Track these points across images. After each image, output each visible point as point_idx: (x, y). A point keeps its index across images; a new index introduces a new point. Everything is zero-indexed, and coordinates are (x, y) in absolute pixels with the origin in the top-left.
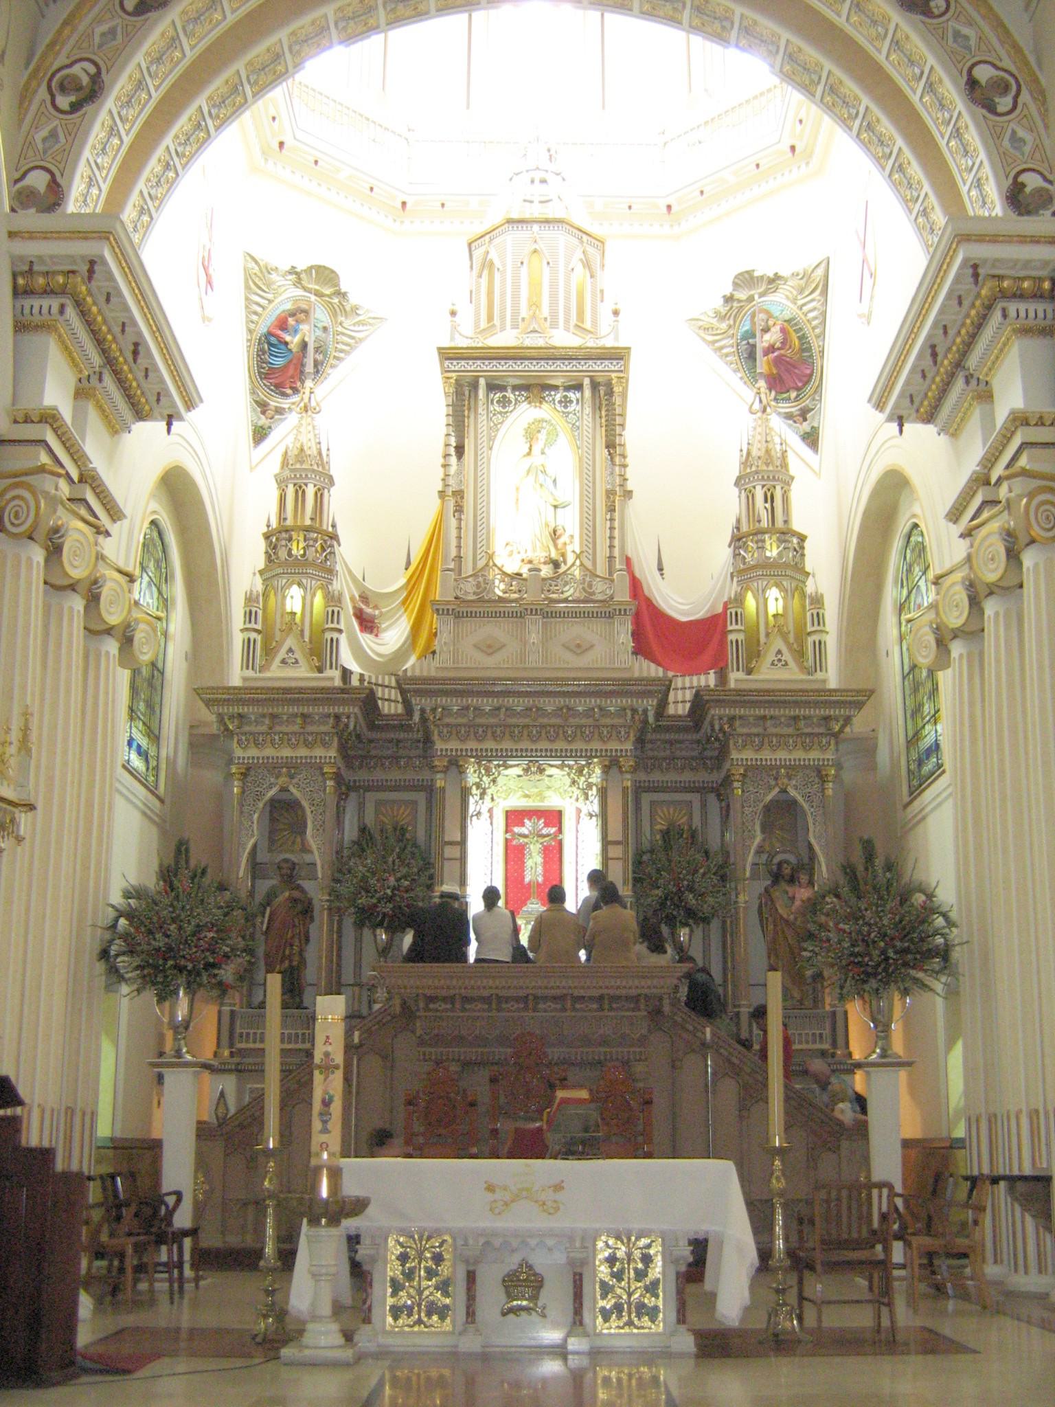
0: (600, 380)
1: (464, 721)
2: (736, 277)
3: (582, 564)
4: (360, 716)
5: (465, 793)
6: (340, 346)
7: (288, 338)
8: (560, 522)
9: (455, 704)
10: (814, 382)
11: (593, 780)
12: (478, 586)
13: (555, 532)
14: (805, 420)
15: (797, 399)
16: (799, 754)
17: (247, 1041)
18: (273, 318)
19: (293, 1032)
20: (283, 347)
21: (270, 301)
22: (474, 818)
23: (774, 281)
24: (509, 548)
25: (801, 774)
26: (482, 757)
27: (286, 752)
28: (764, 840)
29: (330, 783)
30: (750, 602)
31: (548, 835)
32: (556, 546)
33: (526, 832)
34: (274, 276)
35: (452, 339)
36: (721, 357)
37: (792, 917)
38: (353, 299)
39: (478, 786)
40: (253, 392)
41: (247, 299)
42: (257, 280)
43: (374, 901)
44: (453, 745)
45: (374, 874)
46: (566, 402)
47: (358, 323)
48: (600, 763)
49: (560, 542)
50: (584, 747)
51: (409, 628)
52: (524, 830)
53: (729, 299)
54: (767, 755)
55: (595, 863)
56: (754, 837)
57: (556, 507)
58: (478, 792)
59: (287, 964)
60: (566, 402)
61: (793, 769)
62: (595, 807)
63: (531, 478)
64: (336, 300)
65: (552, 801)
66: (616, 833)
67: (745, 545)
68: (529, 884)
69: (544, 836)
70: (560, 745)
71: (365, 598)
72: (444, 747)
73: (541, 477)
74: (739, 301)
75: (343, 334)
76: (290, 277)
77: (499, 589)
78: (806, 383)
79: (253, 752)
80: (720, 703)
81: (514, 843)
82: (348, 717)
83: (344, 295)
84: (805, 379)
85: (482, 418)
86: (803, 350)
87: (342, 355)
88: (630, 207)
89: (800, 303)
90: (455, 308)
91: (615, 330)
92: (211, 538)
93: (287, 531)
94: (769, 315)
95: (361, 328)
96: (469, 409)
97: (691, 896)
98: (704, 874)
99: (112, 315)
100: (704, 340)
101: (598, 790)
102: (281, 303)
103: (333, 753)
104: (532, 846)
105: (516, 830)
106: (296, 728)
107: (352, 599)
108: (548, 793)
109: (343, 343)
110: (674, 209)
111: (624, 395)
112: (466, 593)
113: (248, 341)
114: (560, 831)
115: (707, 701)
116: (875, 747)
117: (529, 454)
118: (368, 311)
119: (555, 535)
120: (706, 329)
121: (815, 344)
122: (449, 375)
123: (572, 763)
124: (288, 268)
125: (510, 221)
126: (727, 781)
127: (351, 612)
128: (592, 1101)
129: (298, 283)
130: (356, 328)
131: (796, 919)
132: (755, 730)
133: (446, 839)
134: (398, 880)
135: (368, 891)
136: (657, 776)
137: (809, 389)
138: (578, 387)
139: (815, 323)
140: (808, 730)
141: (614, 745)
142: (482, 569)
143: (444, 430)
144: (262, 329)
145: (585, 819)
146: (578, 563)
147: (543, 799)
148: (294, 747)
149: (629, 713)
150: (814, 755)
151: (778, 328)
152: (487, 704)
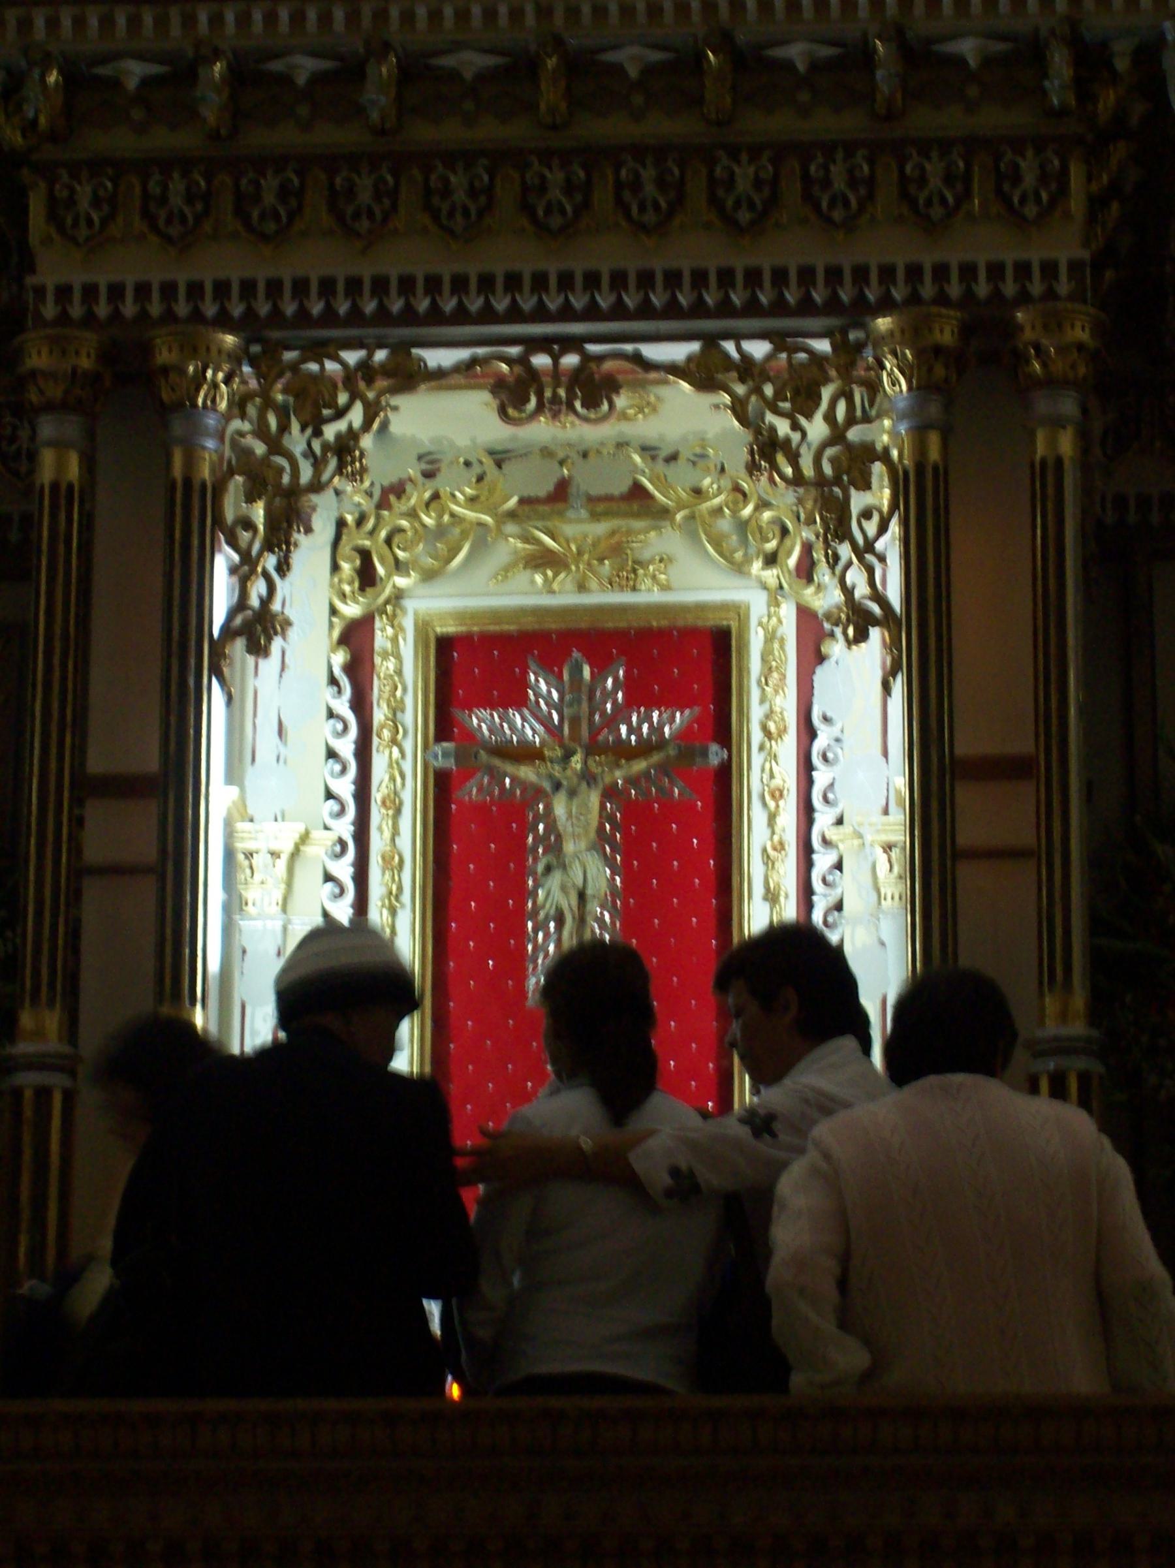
1: (185, 140)
31: (645, 748)
33: (533, 733)
48: (913, 333)
55: (778, 697)
58: (258, 513)
69: (623, 752)
72: (78, 279)
81: (472, 791)
96: (906, 473)
99: (187, 210)
104: (560, 809)
105: (481, 721)
123: (758, 349)
133: (97, 764)
149: (1060, 62)
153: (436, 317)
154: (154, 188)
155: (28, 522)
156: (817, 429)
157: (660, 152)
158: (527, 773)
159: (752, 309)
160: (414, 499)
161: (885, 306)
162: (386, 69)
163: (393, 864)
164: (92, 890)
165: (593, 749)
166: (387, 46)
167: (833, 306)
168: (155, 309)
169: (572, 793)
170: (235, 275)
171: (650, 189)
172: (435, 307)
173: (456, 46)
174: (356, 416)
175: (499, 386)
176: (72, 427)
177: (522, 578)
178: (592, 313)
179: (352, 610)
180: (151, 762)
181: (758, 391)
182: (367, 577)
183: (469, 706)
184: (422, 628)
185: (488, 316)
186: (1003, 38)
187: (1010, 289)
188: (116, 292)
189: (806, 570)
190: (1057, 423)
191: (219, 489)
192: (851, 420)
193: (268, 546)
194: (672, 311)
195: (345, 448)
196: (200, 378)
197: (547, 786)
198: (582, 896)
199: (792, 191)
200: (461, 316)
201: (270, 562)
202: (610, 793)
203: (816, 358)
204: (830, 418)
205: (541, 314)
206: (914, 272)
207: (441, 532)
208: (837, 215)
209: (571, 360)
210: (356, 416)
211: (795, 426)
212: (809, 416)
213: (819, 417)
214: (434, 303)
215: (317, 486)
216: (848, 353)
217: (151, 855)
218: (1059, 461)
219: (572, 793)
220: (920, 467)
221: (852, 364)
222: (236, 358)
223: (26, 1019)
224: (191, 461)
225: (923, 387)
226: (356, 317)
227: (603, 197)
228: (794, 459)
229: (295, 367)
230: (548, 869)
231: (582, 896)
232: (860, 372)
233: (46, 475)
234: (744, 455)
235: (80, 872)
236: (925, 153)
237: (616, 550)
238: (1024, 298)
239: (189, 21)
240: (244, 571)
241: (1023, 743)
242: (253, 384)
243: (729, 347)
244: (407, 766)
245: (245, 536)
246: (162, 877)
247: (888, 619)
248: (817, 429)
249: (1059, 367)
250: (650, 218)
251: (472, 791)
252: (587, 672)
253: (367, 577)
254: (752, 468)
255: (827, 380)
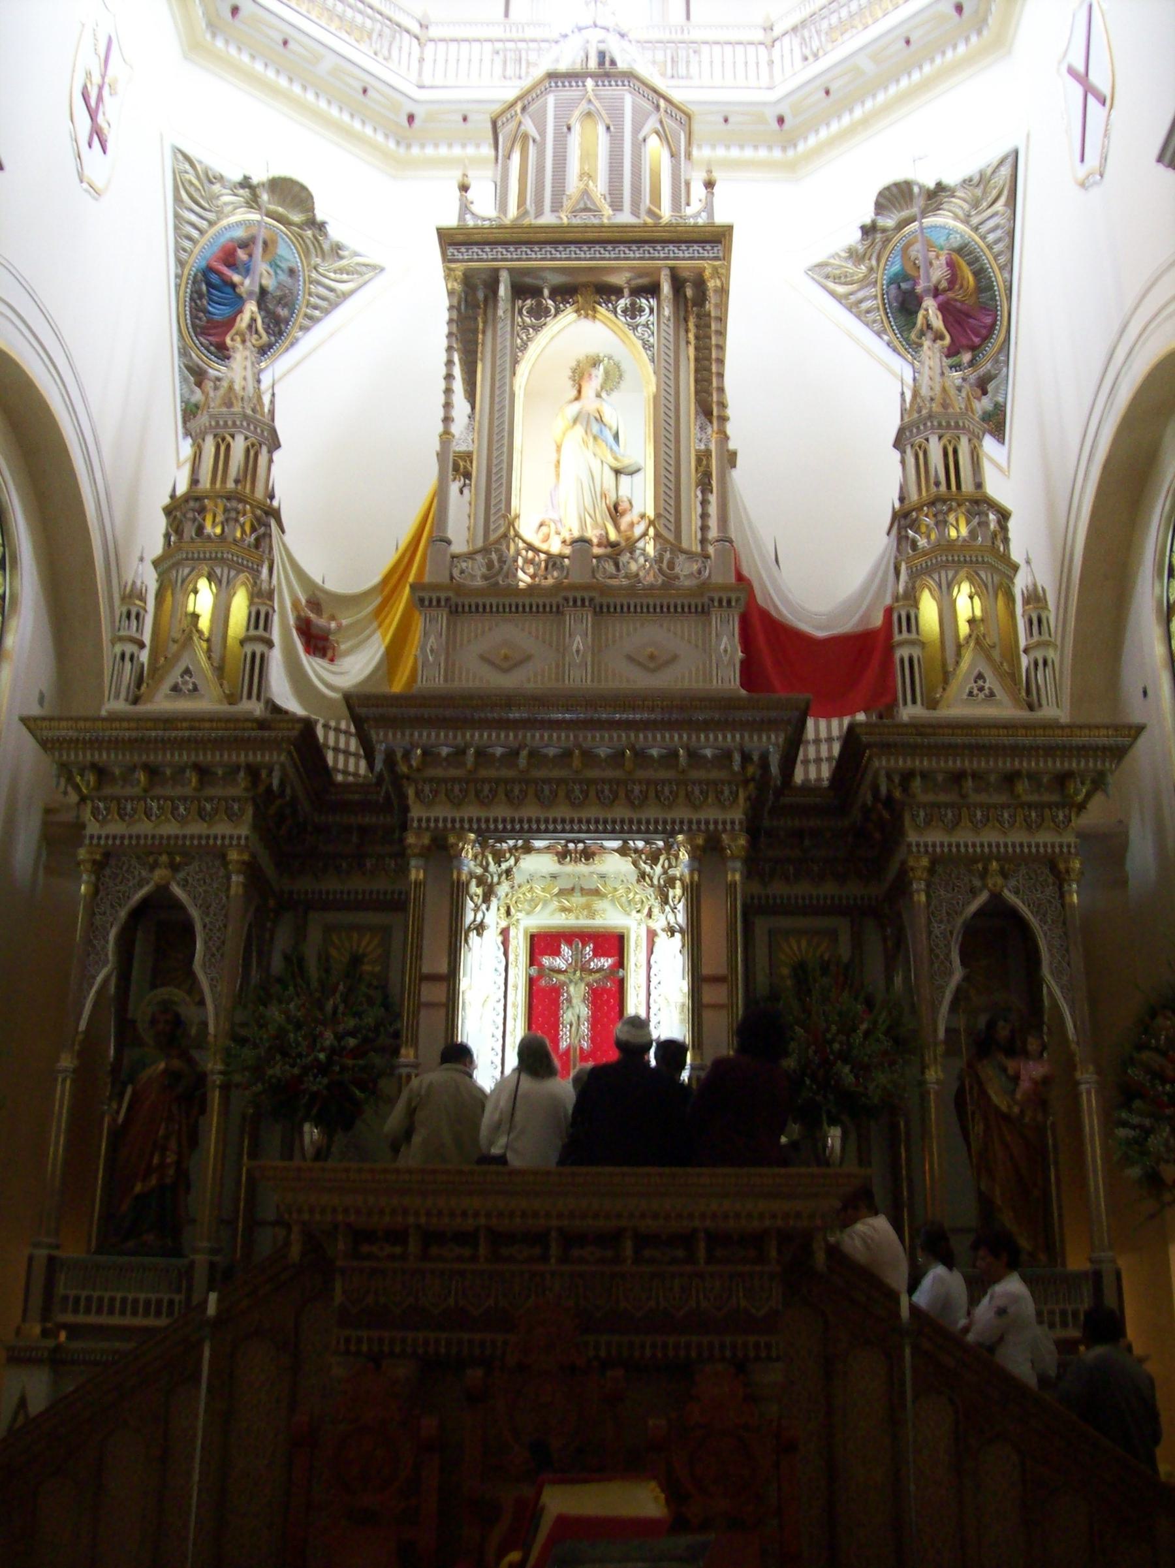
0: (686, 274)
2: (881, 194)
3: (658, 535)
4: (291, 771)
5: (457, 893)
6: (313, 300)
7: (236, 278)
8: (624, 492)
9: (444, 742)
10: (999, 337)
11: (676, 872)
12: (490, 565)
13: (616, 507)
14: (985, 393)
15: (972, 363)
16: (1018, 836)
17: (76, 1311)
18: (215, 249)
19: (153, 1297)
20: (229, 290)
21: (211, 224)
22: (473, 935)
23: (937, 195)
24: (544, 529)
25: (1023, 870)
26: (487, 834)
27: (170, 828)
28: (966, 978)
29: (236, 879)
30: (929, 610)
32: (617, 526)
33: (563, 966)
34: (217, 188)
35: (461, 217)
36: (858, 317)
37: (1016, 1110)
38: (335, 232)
39: (481, 881)
40: (184, 353)
41: (177, 216)
42: (192, 190)
43: (296, 1071)
44: (441, 811)
45: (298, 1026)
46: (633, 311)
47: (341, 271)
48: (690, 840)
49: (624, 522)
50: (661, 815)
51: (382, 649)
52: (559, 963)
53: (868, 231)
54: (964, 837)
56: (951, 973)
57: (617, 472)
58: (479, 891)
59: (153, 1181)
60: (633, 311)
61: (1010, 862)
62: (681, 918)
63: (579, 429)
64: (309, 233)
65: (609, 917)
66: (714, 964)
67: (914, 525)
68: (567, 1051)
69: (592, 972)
70: (621, 812)
71: (315, 604)
72: (424, 815)
73: (595, 427)
74: (884, 230)
75: (319, 283)
76: (241, 192)
77: (524, 579)
78: (986, 338)
79: (117, 828)
80: (887, 748)
81: (543, 983)
82: (271, 771)
83: (321, 227)
84: (984, 332)
85: (504, 327)
86: (979, 290)
87: (317, 313)
88: (726, 120)
89: (975, 221)
90: (467, 181)
91: (709, 207)
92: (82, 513)
93: (197, 499)
94: (929, 245)
95: (345, 277)
97: (847, 1069)
98: (867, 1034)
100: (833, 294)
101: (684, 888)
102: (229, 227)
103: (244, 830)
104: (572, 989)
105: (546, 961)
106: (188, 791)
107: (296, 604)
108: (600, 905)
109: (319, 297)
110: (788, 121)
111: (724, 291)
112: (473, 577)
113: (177, 276)
114: (621, 964)
115: (869, 746)
116: (1124, 846)
117: (578, 398)
118: (356, 254)
119: (616, 512)
120: (836, 279)
121: (999, 279)
122: (453, 265)
124: (238, 178)
125: (552, 76)
126: (901, 887)
127: (292, 621)
128: (678, 1523)
129: (253, 202)
130: (338, 276)
131: (1022, 1112)
132: (943, 798)
133: (426, 969)
134: (339, 1037)
135: (285, 1054)
136: (779, 889)
137: (992, 347)
138: (652, 290)
139: (997, 248)
140: (1034, 798)
141: (711, 813)
142: (498, 541)
143: (444, 343)
144: (196, 261)
145: (662, 940)
146: (651, 531)
147: (592, 914)
148: (183, 821)
149: (737, 757)
150: (1045, 838)
151: (943, 260)
152: (498, 743)
153: (538, 831)
154: (449, 787)
155: (407, 894)
156: (658, 869)
157: (610, 781)
158: (562, 977)
159: (639, 831)
160: (524, 889)
161: (680, 832)
162: (524, 753)
163: (515, 1005)
164: (423, 1013)
165: (583, 970)
166: (526, 745)
167: (664, 832)
168: (720, 827)
169: (576, 984)
170: (441, 815)
171: (607, 792)
172: (522, 828)
173: (547, 746)
174: (512, 861)
175: (557, 854)
176: (421, 862)
177: (557, 915)
178: (588, 831)
179: (503, 924)
180: (444, 969)
181: (641, 857)
182: (508, 913)
183: (544, 953)
184: (525, 932)
185: (555, 831)
186: (718, 749)
187: (720, 827)
188: (437, 820)
189: (650, 915)
190: (734, 870)
191: (468, 883)
192: (670, 866)
193: (484, 902)
194: (613, 831)
195: (508, 872)
196: (463, 848)
197: (568, 981)
198: (579, 1017)
199: (652, 794)
200: (547, 831)
201: (484, 907)
202: (587, 985)
203: (659, 849)
204: (663, 867)
205: (572, 831)
206: (690, 822)
207: (532, 900)
208: (666, 803)
209: (581, 846)
210: (512, 861)
211: (652, 868)
212: (656, 865)
213: (659, 866)
214: (530, 827)
215: (499, 883)
216: (668, 847)
217: (444, 1000)
218: (736, 884)
219: (576, 984)
220: (692, 883)
221: (670, 849)
222: (474, 842)
223: (403, 1051)
224: (459, 874)
225: (693, 857)
226: (513, 830)
227: (592, 793)
228: (651, 880)
229: (493, 846)
230: (568, 1008)
231: (579, 1017)
232: (673, 852)
233: (413, 876)
234: (636, 878)
235: (419, 1006)
236: (694, 784)
237: (588, 907)
238: (725, 830)
239: (464, 736)
240: (477, 909)
241: (723, 971)
242: (479, 850)
243: (631, 843)
244: (520, 974)
245: (475, 898)
246: (447, 1008)
247: (681, 931)
248: (658, 869)
249: (736, 852)
250: (607, 801)
251: (543, 983)
252: (580, 945)
253: (508, 913)
254: (638, 881)
255: (662, 854)
